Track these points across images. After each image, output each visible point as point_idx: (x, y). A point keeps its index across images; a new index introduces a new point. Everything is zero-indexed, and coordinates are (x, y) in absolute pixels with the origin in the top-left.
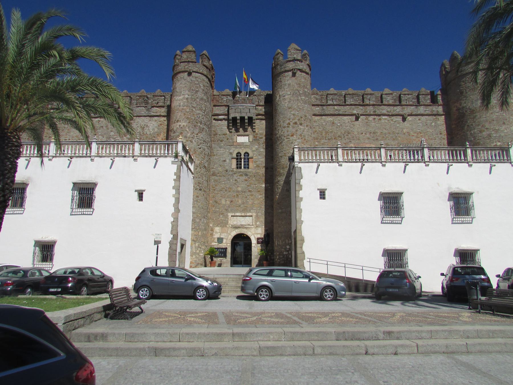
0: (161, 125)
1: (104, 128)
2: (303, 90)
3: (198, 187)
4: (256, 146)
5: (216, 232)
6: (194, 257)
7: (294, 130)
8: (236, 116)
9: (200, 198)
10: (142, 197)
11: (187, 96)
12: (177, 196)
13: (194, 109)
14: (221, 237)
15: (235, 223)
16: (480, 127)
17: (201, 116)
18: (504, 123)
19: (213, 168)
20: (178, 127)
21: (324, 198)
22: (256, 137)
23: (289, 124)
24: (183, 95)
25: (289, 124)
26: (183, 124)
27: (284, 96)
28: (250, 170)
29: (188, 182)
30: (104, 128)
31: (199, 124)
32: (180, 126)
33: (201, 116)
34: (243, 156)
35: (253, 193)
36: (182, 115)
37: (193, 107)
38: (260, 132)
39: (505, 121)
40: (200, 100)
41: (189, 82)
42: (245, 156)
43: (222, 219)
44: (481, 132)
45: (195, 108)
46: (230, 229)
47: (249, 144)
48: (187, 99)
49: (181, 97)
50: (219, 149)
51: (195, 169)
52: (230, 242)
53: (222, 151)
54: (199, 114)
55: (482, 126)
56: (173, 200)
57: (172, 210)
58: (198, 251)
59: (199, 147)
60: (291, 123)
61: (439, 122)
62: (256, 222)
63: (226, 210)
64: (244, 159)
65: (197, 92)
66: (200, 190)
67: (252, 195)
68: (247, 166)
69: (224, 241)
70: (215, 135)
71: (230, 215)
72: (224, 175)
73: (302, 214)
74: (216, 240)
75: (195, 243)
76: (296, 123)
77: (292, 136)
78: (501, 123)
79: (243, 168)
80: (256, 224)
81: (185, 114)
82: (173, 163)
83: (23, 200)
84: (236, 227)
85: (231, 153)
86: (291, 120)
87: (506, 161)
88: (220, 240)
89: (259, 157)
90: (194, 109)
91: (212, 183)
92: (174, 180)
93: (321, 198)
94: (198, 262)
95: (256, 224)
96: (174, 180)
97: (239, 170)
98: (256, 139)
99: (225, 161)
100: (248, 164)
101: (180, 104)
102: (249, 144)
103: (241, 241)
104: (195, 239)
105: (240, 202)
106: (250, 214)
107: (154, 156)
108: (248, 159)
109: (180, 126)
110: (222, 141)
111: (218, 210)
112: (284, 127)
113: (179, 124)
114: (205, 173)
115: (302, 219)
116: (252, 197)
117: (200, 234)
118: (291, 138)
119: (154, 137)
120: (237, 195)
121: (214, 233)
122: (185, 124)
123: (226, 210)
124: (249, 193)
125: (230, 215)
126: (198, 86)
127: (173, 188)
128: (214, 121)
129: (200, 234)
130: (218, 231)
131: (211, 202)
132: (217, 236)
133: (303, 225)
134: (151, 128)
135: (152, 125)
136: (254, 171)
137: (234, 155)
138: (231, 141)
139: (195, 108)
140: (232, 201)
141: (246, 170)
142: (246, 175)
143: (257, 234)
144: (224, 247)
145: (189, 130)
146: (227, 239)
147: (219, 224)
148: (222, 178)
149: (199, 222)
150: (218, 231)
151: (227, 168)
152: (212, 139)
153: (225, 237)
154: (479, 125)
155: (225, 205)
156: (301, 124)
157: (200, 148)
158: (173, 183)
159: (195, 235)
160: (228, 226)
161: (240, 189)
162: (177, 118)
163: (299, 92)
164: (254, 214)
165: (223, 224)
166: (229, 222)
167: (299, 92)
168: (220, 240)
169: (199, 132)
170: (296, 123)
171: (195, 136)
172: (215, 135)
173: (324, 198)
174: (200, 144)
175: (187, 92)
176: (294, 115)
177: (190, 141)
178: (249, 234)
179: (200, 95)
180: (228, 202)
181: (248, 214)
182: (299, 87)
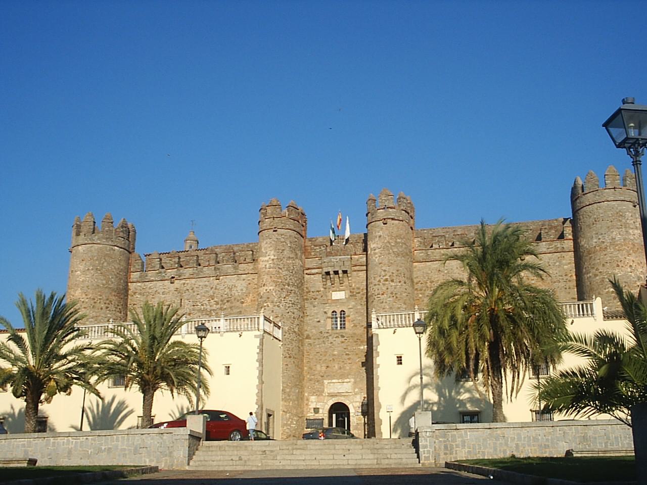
0: (249, 284)
1: (190, 291)
2: (396, 242)
3: (287, 355)
4: (353, 303)
5: (312, 402)
6: (285, 428)
7: (384, 288)
8: (329, 270)
9: (289, 366)
10: (229, 371)
11: (272, 257)
12: (261, 368)
13: (281, 271)
14: (318, 407)
15: (332, 391)
16: (594, 270)
17: (288, 277)
18: (618, 266)
19: (306, 331)
20: (265, 291)
21: (401, 363)
22: (353, 292)
23: (379, 281)
24: (269, 255)
25: (379, 281)
26: (270, 288)
27: (375, 250)
28: (346, 330)
29: (277, 350)
30: (190, 291)
31: (287, 287)
32: (266, 290)
33: (288, 277)
34: (338, 315)
35: (350, 356)
36: (269, 278)
37: (279, 268)
38: (357, 286)
39: (619, 264)
40: (287, 260)
41: (274, 241)
42: (341, 314)
43: (318, 386)
44: (596, 275)
45: (281, 269)
46: (326, 398)
47: (345, 301)
48: (273, 260)
49: (267, 258)
50: (313, 308)
51: (283, 335)
52: (327, 413)
53: (315, 310)
54: (287, 275)
55: (596, 270)
56: (257, 373)
57: (257, 382)
58: (289, 422)
59: (287, 311)
60: (382, 281)
61: (564, 262)
62: (354, 389)
63: (322, 376)
64: (341, 318)
65: (283, 250)
66: (290, 357)
67: (349, 359)
68: (343, 326)
69: (321, 411)
70: (307, 293)
71: (326, 382)
72: (319, 337)
73: (379, 380)
74: (312, 411)
75: (286, 414)
76: (386, 280)
77: (383, 294)
78: (615, 265)
79: (339, 328)
80: (354, 391)
81: (271, 277)
82: (256, 336)
83: (496, 462)
84: (332, 395)
85: (325, 313)
86: (381, 277)
87: (590, 315)
88: (316, 410)
89: (357, 315)
90: (281, 271)
91: (306, 348)
92: (258, 353)
93: (398, 364)
94: (290, 433)
95: (354, 391)
96: (258, 353)
97: (335, 331)
98: (352, 295)
99: (319, 322)
100: (344, 324)
101: (266, 265)
102: (345, 301)
103: (340, 410)
104: (285, 410)
105: (336, 367)
106: (348, 380)
107: (238, 331)
108: (344, 317)
109: (266, 290)
110: (315, 299)
111: (313, 377)
112: (375, 285)
113: (266, 288)
114: (295, 339)
115: (379, 386)
116: (350, 362)
117: (291, 404)
118: (382, 297)
119: (243, 299)
120: (333, 359)
121: (310, 403)
122: (272, 288)
123: (322, 376)
124: (347, 357)
125: (326, 382)
126: (284, 243)
127: (257, 361)
128: (307, 276)
129: (291, 404)
130: (314, 401)
131: (305, 368)
132: (313, 406)
133: (380, 391)
134: (239, 288)
135: (240, 284)
136: (351, 332)
137: (330, 314)
138: (325, 298)
139: (281, 269)
140: (327, 367)
141: (343, 331)
142: (343, 336)
143: (356, 402)
144: (320, 418)
145: (276, 295)
146: (323, 409)
147: (314, 393)
148: (317, 342)
149: (289, 392)
150: (314, 401)
151: (322, 329)
152: (305, 297)
153: (319, 407)
154: (593, 268)
155: (321, 371)
156: (392, 281)
157: (288, 313)
158: (256, 357)
159: (286, 406)
160: (324, 394)
161: (336, 353)
162: (263, 281)
163: (390, 244)
164: (352, 380)
165: (319, 393)
166: (326, 390)
167: (390, 244)
168: (316, 410)
169: (287, 295)
170: (386, 280)
171: (283, 299)
172: (307, 293)
173: (401, 363)
174: (289, 307)
175: (272, 252)
176: (385, 271)
177: (277, 305)
178: (347, 403)
179: (287, 253)
180: (324, 368)
181: (345, 381)
182: (391, 239)
